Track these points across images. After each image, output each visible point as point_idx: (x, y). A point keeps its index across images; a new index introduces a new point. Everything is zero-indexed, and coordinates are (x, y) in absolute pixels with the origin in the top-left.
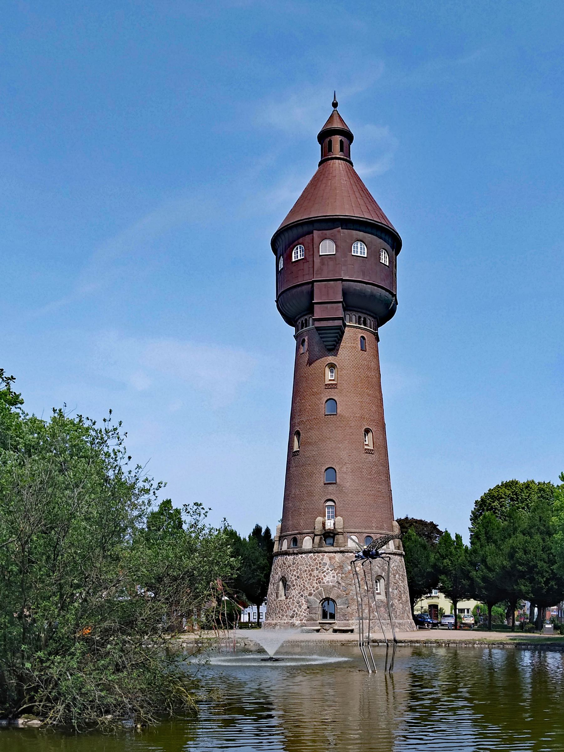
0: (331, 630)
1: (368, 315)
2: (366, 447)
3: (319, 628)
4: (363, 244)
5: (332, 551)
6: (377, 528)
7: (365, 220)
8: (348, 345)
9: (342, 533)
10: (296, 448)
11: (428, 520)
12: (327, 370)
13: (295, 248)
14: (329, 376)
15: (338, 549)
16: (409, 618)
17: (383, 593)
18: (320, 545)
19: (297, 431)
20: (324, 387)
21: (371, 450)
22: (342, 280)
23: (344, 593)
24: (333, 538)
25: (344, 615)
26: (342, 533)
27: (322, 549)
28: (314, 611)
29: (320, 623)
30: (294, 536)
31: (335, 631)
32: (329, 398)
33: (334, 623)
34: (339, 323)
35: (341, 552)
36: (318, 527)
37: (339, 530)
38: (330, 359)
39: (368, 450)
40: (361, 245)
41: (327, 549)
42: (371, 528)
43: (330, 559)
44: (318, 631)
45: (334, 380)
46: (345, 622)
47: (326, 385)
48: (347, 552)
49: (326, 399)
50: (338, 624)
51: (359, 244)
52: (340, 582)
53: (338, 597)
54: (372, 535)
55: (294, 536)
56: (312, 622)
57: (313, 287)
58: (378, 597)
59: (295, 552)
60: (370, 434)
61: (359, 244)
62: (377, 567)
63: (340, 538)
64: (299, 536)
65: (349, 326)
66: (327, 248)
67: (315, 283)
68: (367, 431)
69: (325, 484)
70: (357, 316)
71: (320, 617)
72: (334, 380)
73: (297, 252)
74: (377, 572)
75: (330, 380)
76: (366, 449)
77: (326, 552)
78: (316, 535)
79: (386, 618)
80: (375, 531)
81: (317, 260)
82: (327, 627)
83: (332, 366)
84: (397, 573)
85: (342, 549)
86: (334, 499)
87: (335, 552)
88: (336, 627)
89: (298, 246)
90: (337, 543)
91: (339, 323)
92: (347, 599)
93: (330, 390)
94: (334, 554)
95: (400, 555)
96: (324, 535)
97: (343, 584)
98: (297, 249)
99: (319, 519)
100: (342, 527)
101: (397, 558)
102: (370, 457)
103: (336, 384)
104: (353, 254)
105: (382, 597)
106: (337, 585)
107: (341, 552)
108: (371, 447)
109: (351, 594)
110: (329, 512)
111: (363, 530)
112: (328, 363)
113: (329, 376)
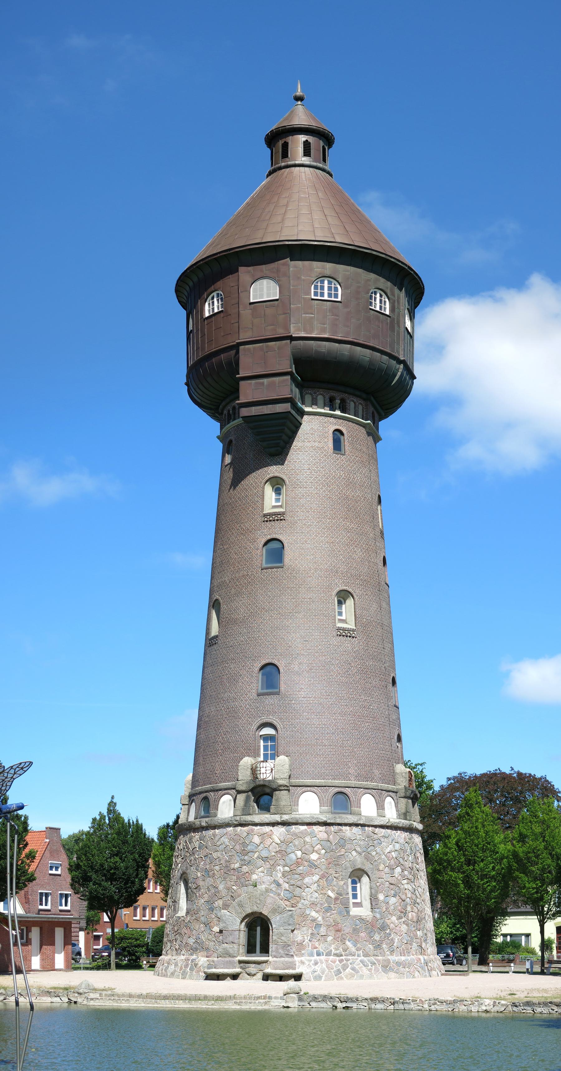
0: (260, 975)
1: (350, 394)
2: (340, 625)
3: (238, 970)
4: (384, 296)
5: (267, 821)
6: (358, 777)
7: (353, 248)
8: (308, 444)
9: (287, 788)
10: (215, 630)
11: (492, 769)
12: (268, 490)
13: (210, 297)
14: (270, 500)
15: (277, 818)
16: (422, 951)
17: (367, 904)
18: (246, 811)
19: (217, 600)
20: (260, 519)
21: (349, 630)
22: (292, 338)
23: (288, 903)
24: (271, 795)
25: (286, 946)
26: (287, 788)
27: (249, 818)
28: (230, 939)
29: (240, 962)
30: (205, 795)
31: (266, 977)
32: (269, 537)
33: (266, 962)
34: (286, 407)
35: (284, 824)
36: (244, 776)
37: (281, 782)
38: (273, 470)
39: (344, 630)
40: (381, 296)
41: (257, 818)
42: (346, 777)
43: (262, 835)
44: (235, 977)
45: (281, 506)
46: (287, 959)
47: (265, 515)
48: (296, 824)
49: (264, 540)
50: (274, 963)
51: (326, 282)
52: (281, 881)
53: (274, 911)
54: (347, 791)
55: (205, 795)
56: (228, 959)
57: (238, 352)
58: (354, 911)
59: (204, 824)
60: (350, 602)
61: (326, 282)
62: (354, 853)
63: (282, 797)
64: (212, 794)
65: (310, 414)
66: (263, 290)
67: (241, 348)
68: (343, 596)
69: (258, 695)
70: (327, 397)
71: (243, 950)
72: (281, 506)
73: (213, 303)
74: (353, 862)
75: (274, 507)
76: (339, 629)
77: (256, 825)
78: (239, 792)
79: (371, 953)
80: (353, 783)
81: (246, 313)
82: (252, 968)
83: (277, 484)
84: (399, 864)
85: (285, 817)
86: (275, 723)
87: (273, 824)
88: (269, 970)
89: (215, 294)
90: (277, 806)
91: (286, 407)
92: (291, 916)
93: (273, 523)
94: (271, 828)
95: (410, 830)
96: (252, 790)
97: (286, 886)
98: (213, 298)
99: (247, 761)
100: (286, 775)
101: (401, 836)
102: (347, 643)
103: (283, 514)
104: (313, 297)
105: (364, 912)
106: (273, 887)
107: (284, 824)
108: (351, 626)
109: (300, 905)
110: (266, 748)
111: (330, 782)
112: (268, 476)
113: (270, 500)
